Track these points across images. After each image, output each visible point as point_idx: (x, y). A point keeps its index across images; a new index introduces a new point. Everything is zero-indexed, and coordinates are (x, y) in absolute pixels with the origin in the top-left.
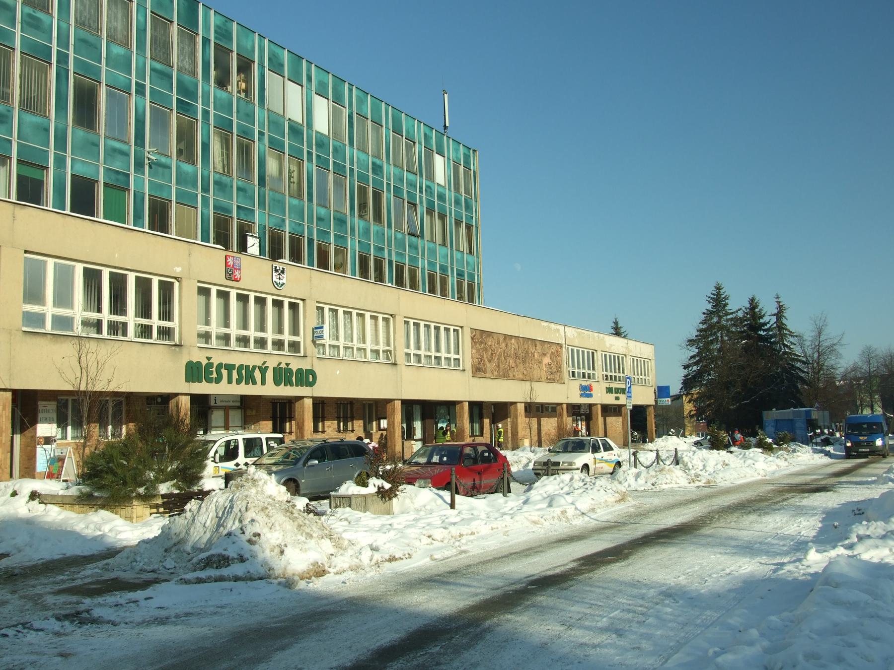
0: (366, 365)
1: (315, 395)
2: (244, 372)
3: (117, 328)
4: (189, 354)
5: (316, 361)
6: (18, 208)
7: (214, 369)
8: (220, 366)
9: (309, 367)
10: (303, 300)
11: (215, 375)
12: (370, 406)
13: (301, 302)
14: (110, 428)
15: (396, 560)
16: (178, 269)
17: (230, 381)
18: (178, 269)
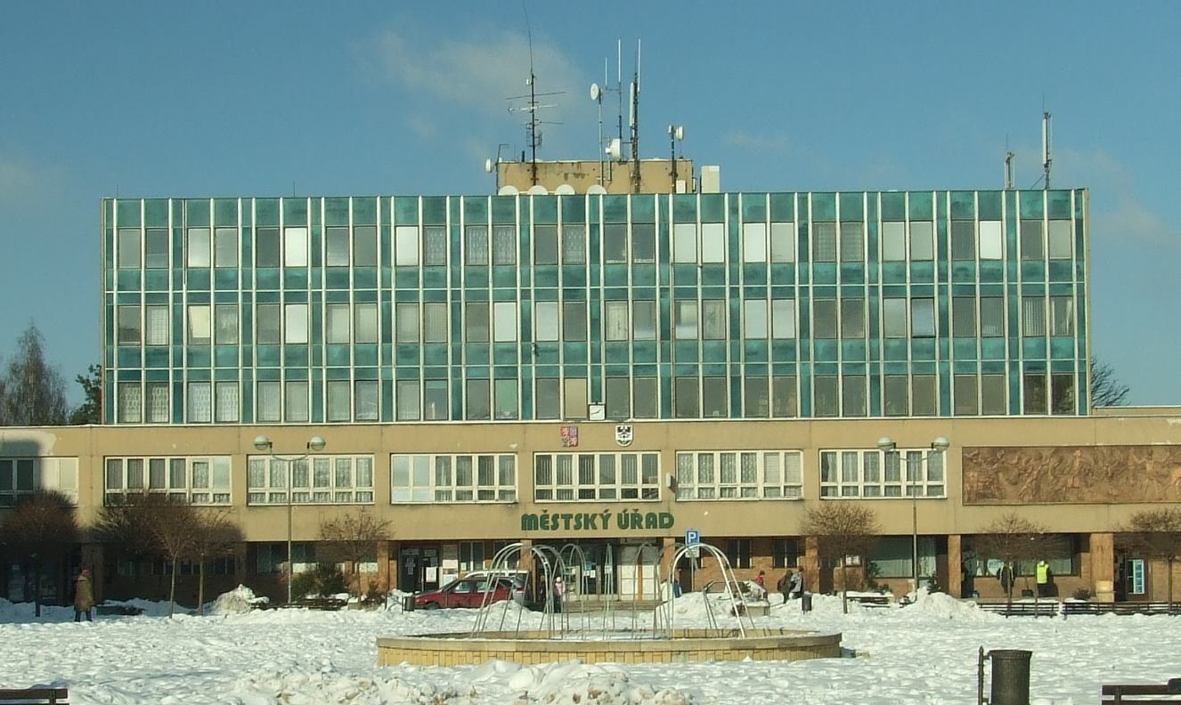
0: (755, 504)
1: (677, 536)
2: (582, 520)
3: (892, 490)
4: (525, 509)
5: (673, 505)
6: (384, 428)
7: (550, 519)
8: (556, 517)
9: (665, 511)
10: (104, 457)
11: (551, 523)
12: (481, 543)
13: (106, 458)
14: (472, 563)
15: (841, 653)
16: (514, 446)
17: (567, 527)
18: (514, 446)
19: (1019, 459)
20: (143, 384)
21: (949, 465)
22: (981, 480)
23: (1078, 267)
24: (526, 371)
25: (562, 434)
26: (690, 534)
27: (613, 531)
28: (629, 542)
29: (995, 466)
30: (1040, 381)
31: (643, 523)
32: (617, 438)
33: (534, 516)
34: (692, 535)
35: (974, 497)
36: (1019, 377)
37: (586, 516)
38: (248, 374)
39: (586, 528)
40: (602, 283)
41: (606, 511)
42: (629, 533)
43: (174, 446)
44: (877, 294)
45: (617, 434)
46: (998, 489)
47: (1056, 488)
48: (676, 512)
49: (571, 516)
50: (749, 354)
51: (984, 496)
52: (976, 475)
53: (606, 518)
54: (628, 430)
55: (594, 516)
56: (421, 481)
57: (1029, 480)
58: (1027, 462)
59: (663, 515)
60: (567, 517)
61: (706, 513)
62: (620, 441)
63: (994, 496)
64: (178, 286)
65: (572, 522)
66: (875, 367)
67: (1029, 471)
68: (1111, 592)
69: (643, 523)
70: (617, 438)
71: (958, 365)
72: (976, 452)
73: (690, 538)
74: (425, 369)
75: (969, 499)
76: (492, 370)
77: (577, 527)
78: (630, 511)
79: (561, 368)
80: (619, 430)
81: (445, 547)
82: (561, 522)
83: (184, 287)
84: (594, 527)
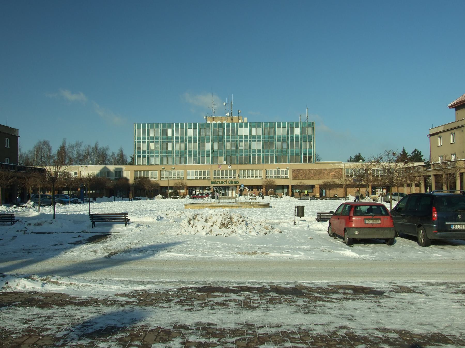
21: (289, 172)
27: (228, 184)
35: (294, 178)
38: (161, 156)
42: (231, 185)
53: (226, 182)
66: (276, 154)
71: (291, 154)
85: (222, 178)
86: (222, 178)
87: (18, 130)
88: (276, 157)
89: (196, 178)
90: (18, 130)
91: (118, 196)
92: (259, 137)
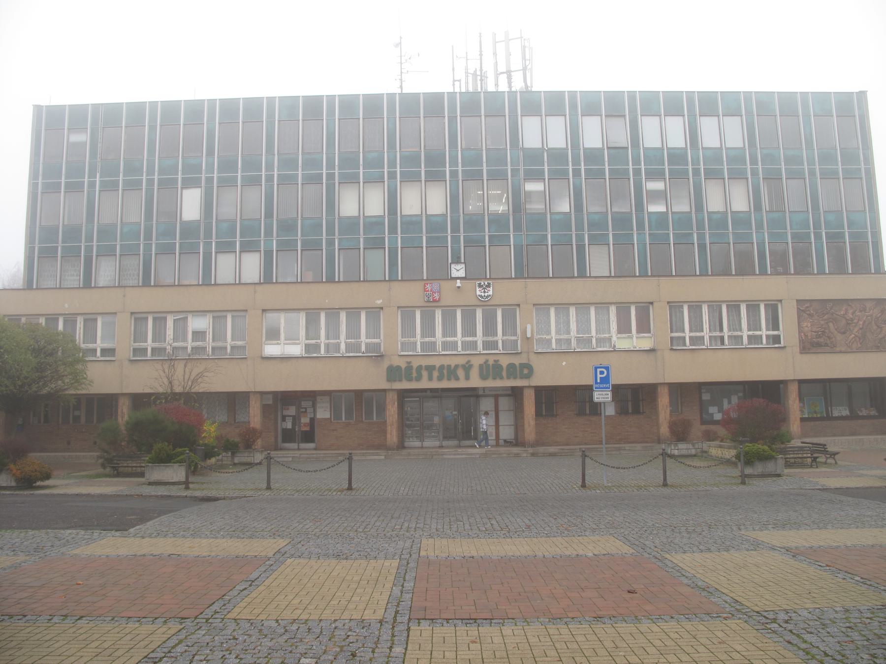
2: (445, 372)
8: (420, 368)
9: (524, 361)
17: (430, 379)
19: (846, 310)
20: (59, 258)
21: (788, 317)
22: (814, 329)
23: (864, 154)
24: (393, 241)
25: (425, 290)
26: (598, 370)
27: (475, 382)
28: (487, 392)
29: (826, 317)
30: (841, 251)
31: (504, 374)
32: (478, 293)
33: (399, 367)
34: (602, 373)
35: (809, 346)
36: (822, 246)
37: (449, 366)
38: (148, 247)
39: (449, 379)
40: (460, 165)
41: (469, 361)
42: (490, 383)
43: (66, 306)
44: (700, 175)
45: (478, 289)
46: (829, 338)
47: (880, 336)
48: (535, 362)
49: (433, 367)
50: (591, 225)
51: (818, 345)
52: (809, 325)
53: (467, 368)
54: (489, 286)
55: (457, 366)
56: (292, 339)
57: (856, 330)
58: (853, 313)
59: (524, 366)
60: (430, 369)
61: (564, 363)
62: (481, 296)
63: (826, 345)
64: (92, 174)
65: (436, 374)
66: (701, 237)
67: (855, 321)
68: (172, 389)
69: (504, 374)
70: (478, 293)
71: (771, 235)
72: (808, 305)
73: (599, 376)
74: (302, 241)
75: (804, 348)
76: (362, 240)
77: (440, 379)
78: (491, 362)
79: (424, 238)
80: (480, 286)
81: (319, 398)
82: (425, 374)
83: (98, 175)
84: (457, 379)
85: (445, 345)
86: (445, 345)
87: (51, 123)
88: (702, 247)
89: (308, 347)
90: (51, 123)
91: (124, 413)
92: (736, 157)
